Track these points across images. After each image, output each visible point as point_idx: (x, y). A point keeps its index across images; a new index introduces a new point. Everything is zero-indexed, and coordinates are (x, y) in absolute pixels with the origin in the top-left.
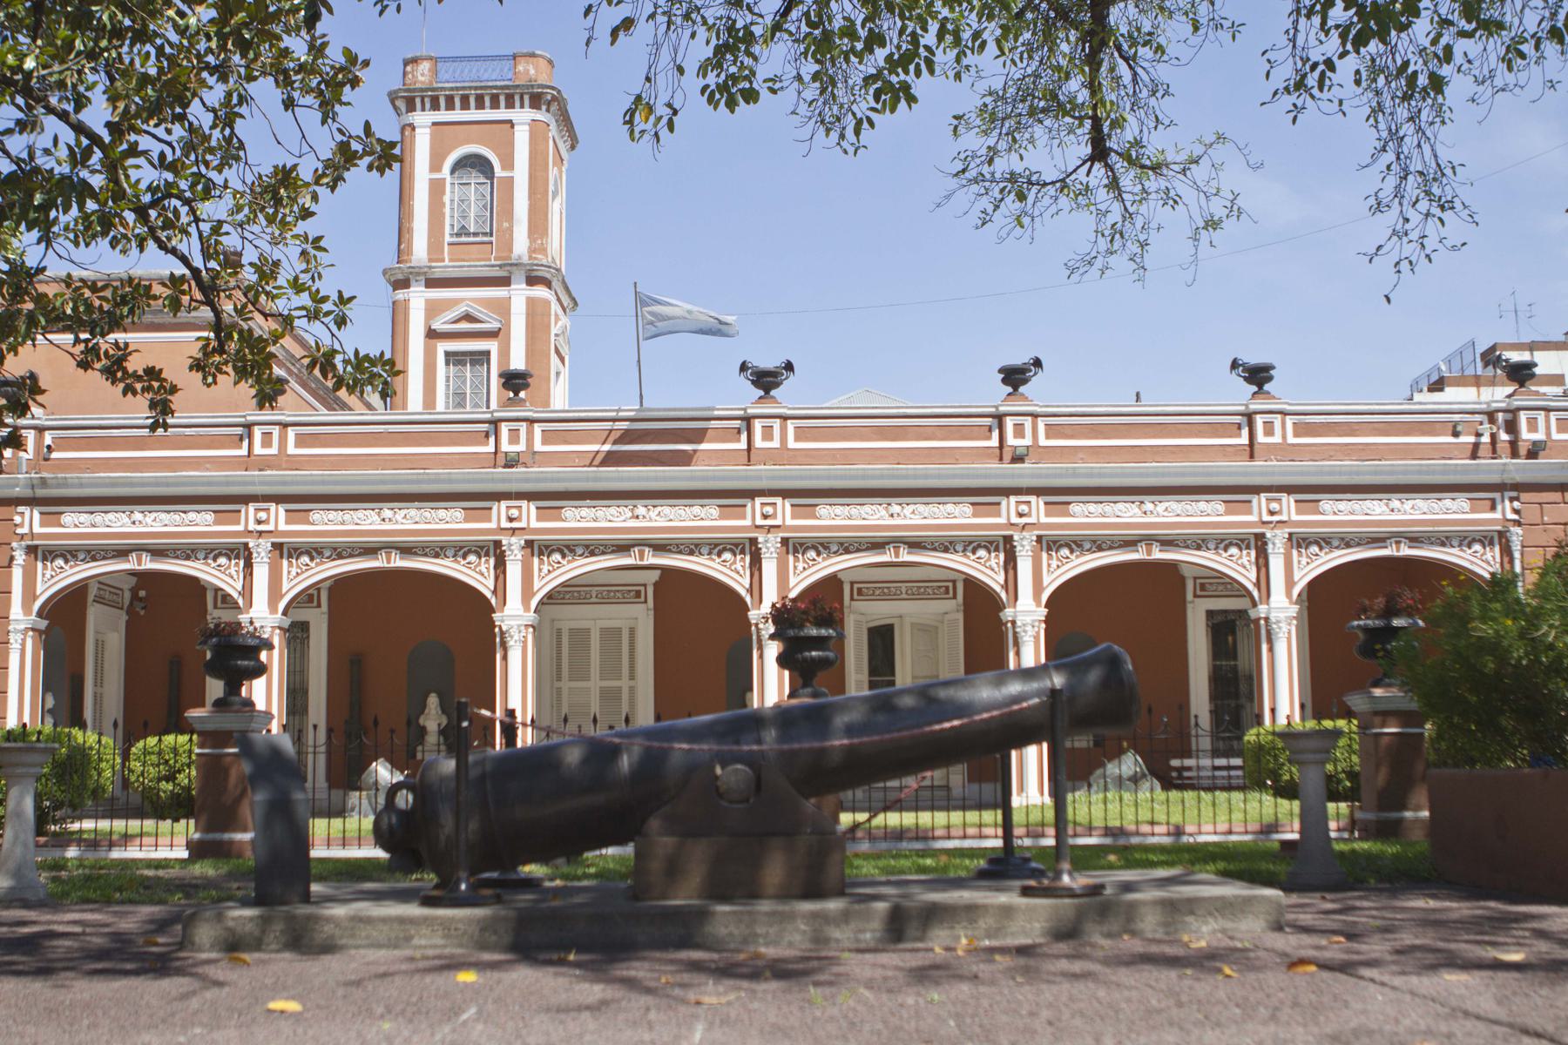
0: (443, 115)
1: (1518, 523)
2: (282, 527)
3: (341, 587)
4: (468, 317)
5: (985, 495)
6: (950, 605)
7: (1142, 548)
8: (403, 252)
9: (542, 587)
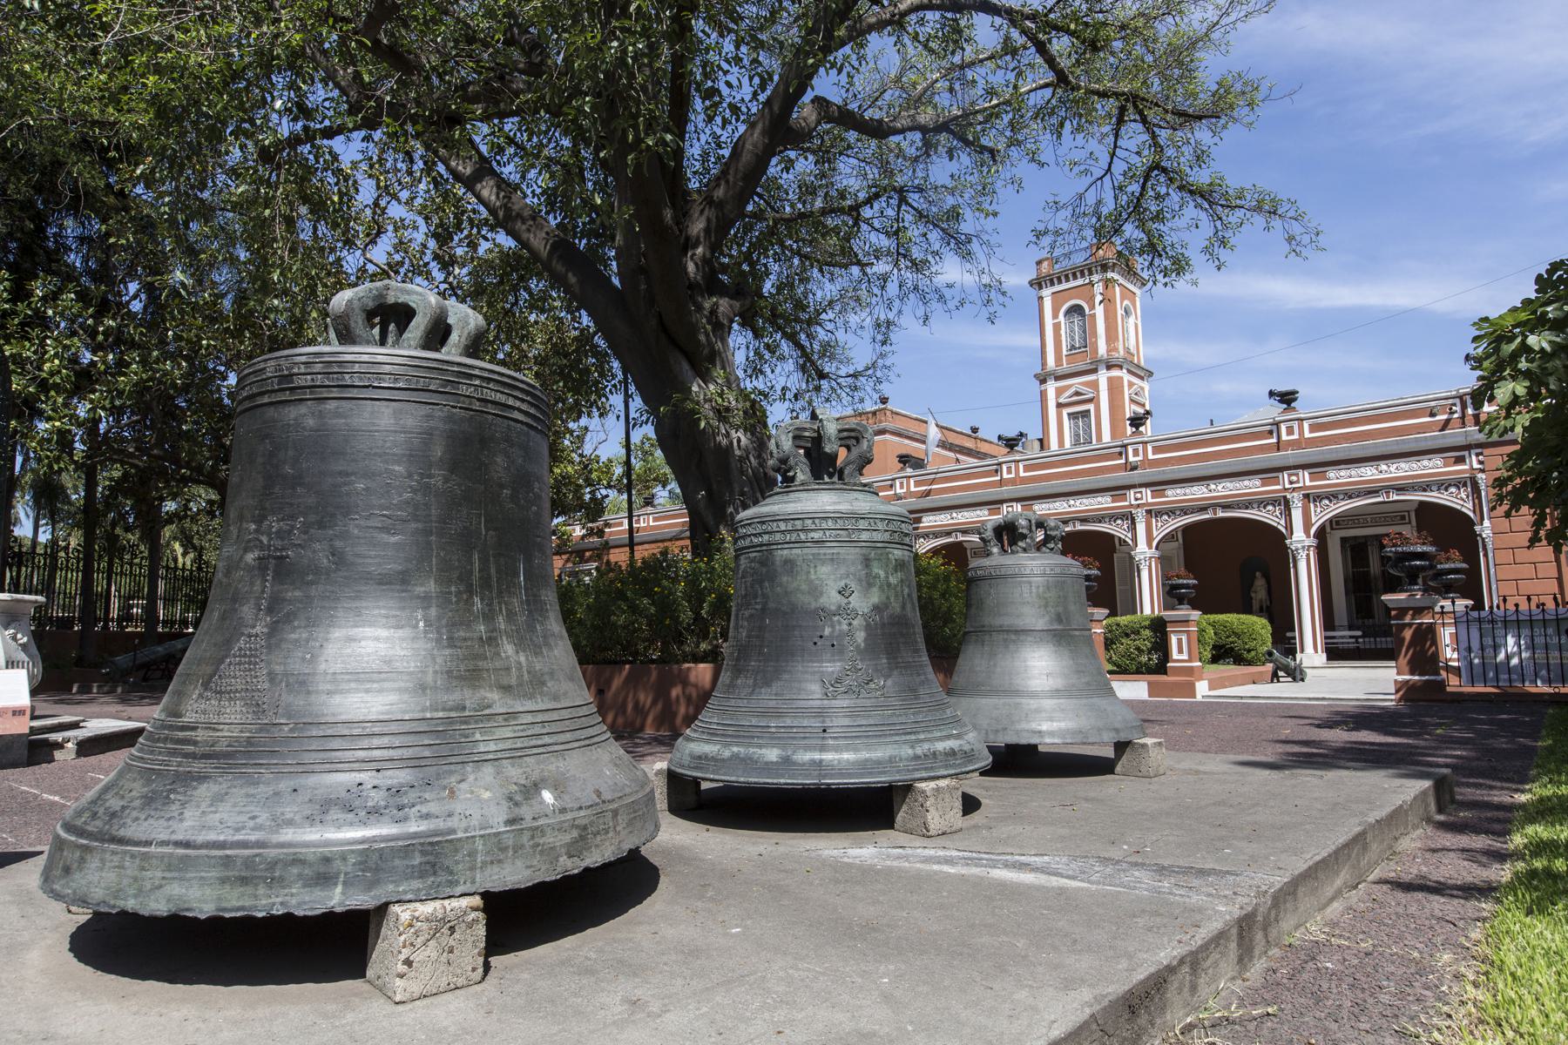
0: (1057, 288)
1: (1482, 471)
2: (1308, 483)
3: (1187, 530)
4: (1077, 394)
5: (1118, 490)
6: (1175, 545)
7: (1210, 511)
8: (1044, 364)
9: (1158, 535)
